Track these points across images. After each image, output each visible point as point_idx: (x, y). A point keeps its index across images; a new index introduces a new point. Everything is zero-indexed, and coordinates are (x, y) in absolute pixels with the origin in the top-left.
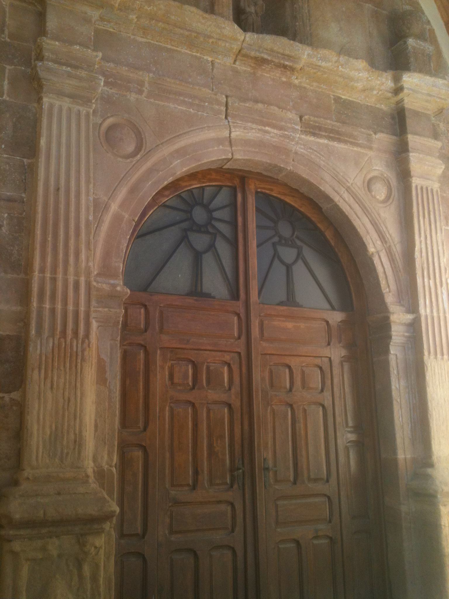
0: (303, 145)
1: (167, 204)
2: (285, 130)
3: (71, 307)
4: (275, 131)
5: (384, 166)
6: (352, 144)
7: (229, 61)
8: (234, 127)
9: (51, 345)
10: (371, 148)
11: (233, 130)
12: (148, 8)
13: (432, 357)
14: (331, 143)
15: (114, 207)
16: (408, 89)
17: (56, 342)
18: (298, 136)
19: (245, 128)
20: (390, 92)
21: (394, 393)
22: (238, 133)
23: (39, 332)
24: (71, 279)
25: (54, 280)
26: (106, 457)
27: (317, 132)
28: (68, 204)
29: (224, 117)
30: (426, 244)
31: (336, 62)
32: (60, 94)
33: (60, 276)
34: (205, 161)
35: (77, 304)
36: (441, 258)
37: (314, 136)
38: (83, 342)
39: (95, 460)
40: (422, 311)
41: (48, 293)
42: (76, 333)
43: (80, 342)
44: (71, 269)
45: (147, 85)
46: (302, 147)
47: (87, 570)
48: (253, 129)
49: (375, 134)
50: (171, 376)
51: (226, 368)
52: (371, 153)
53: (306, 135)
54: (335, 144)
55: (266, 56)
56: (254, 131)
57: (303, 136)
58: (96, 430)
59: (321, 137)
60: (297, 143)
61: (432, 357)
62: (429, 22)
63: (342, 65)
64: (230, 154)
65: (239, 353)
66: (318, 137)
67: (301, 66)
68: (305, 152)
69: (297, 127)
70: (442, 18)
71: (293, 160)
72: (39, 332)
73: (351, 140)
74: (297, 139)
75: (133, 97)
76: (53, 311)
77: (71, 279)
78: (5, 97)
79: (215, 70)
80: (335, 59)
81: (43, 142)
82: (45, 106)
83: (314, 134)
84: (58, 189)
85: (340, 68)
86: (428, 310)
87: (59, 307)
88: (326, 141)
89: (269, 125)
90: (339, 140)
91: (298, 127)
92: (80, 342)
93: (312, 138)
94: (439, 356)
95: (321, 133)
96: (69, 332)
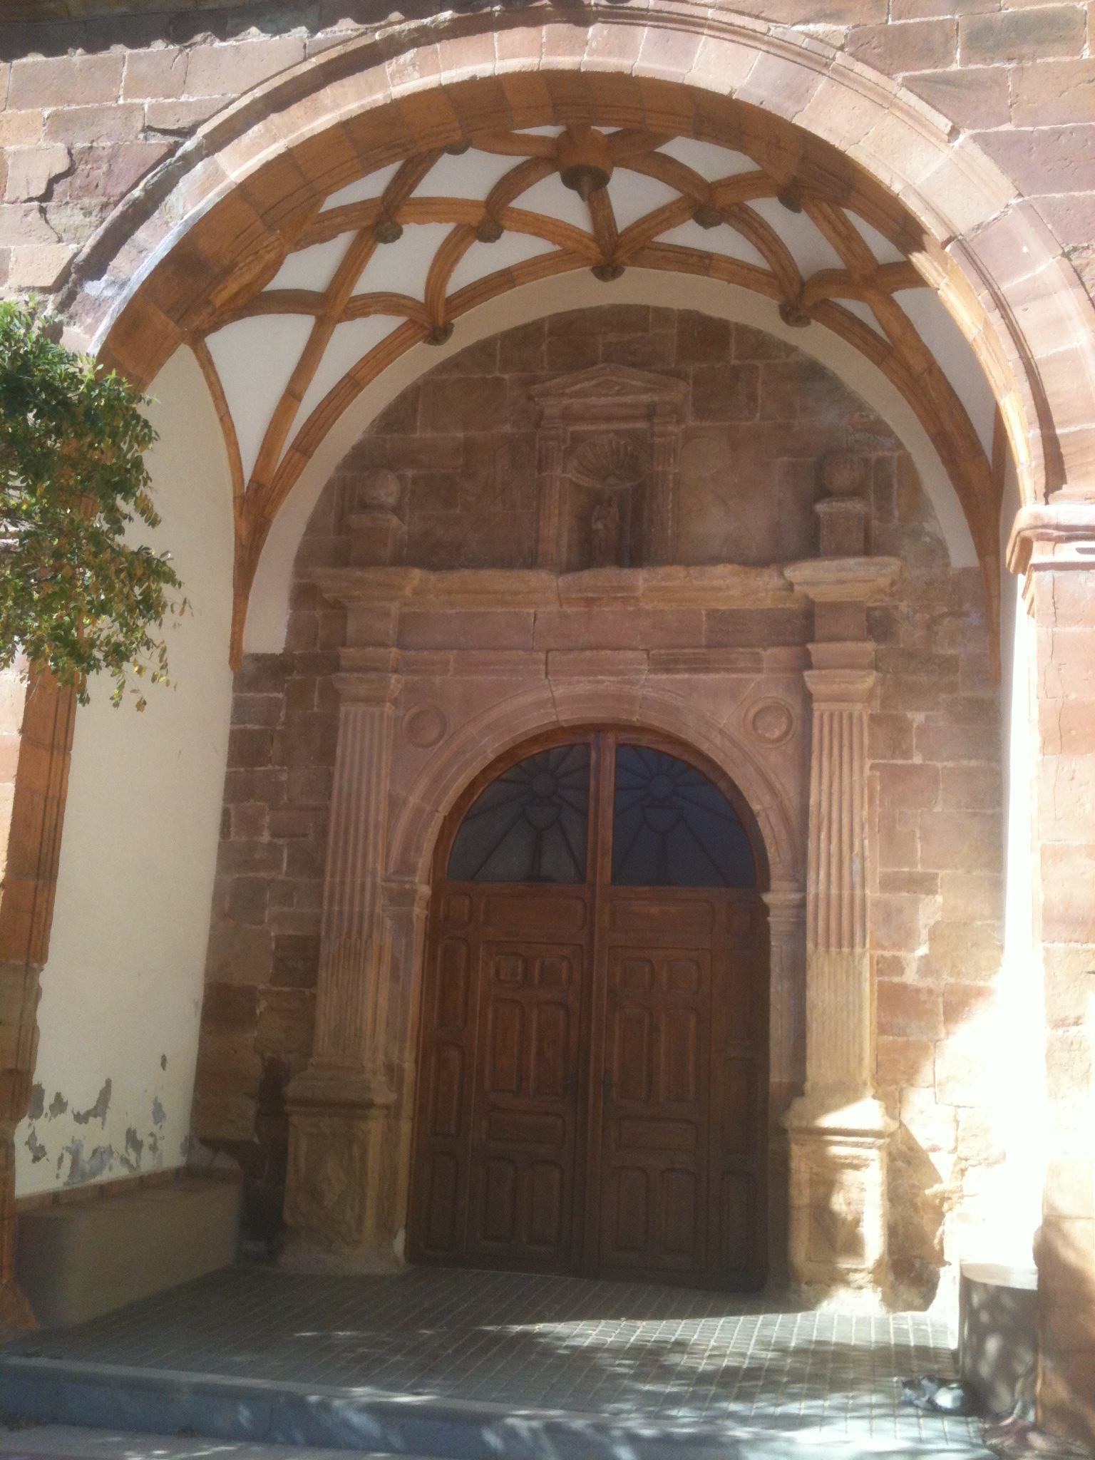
0: (652, 687)
1: (504, 777)
2: (625, 675)
3: (357, 909)
4: (612, 678)
5: (781, 690)
6: (727, 670)
7: (554, 608)
8: (556, 685)
9: (338, 944)
10: (759, 670)
11: (554, 689)
12: (757, 368)
13: (822, 949)
14: (695, 676)
15: (413, 800)
16: (799, 584)
17: (342, 943)
18: (644, 677)
19: (570, 684)
20: (785, 590)
21: (773, 998)
22: (561, 691)
23: (328, 933)
24: (358, 881)
25: (343, 883)
26: (396, 1052)
27: (672, 666)
28: (358, 809)
29: (543, 676)
30: (830, 794)
31: (685, 577)
32: (357, 699)
33: (348, 880)
34: (522, 730)
35: (362, 904)
36: (856, 811)
37: (668, 673)
38: (366, 942)
39: (386, 1053)
40: (811, 890)
41: (337, 896)
42: (360, 932)
43: (364, 942)
44: (359, 871)
45: (452, 663)
46: (650, 689)
47: (356, 1151)
48: (581, 682)
49: (765, 650)
50: (497, 973)
51: (565, 964)
52: (758, 677)
53: (656, 674)
54: (702, 676)
55: (590, 595)
56: (582, 684)
57: (652, 676)
58: (387, 1026)
59: (678, 671)
60: (643, 686)
61: (822, 949)
62: (899, 445)
63: (696, 578)
64: (554, 717)
65: (581, 946)
66: (673, 673)
67: (641, 592)
68: (656, 695)
69: (642, 667)
70: (927, 430)
71: (640, 707)
72: (328, 933)
73: (724, 666)
74: (642, 682)
75: (437, 679)
76: (341, 913)
77: (358, 881)
78: (316, 709)
79: (537, 621)
80: (682, 575)
81: (339, 750)
82: (342, 716)
83: (667, 671)
84: (350, 795)
85: (694, 581)
86: (822, 887)
87: (346, 908)
88: (686, 676)
89: (602, 673)
90: (707, 670)
91: (645, 667)
92: (364, 942)
93: (665, 676)
94: (833, 950)
95: (678, 667)
96: (354, 932)
